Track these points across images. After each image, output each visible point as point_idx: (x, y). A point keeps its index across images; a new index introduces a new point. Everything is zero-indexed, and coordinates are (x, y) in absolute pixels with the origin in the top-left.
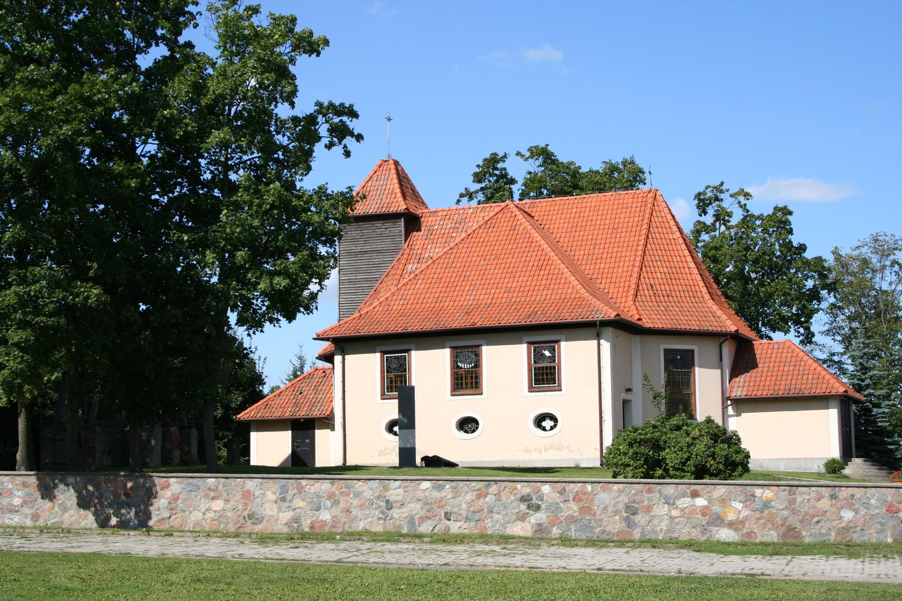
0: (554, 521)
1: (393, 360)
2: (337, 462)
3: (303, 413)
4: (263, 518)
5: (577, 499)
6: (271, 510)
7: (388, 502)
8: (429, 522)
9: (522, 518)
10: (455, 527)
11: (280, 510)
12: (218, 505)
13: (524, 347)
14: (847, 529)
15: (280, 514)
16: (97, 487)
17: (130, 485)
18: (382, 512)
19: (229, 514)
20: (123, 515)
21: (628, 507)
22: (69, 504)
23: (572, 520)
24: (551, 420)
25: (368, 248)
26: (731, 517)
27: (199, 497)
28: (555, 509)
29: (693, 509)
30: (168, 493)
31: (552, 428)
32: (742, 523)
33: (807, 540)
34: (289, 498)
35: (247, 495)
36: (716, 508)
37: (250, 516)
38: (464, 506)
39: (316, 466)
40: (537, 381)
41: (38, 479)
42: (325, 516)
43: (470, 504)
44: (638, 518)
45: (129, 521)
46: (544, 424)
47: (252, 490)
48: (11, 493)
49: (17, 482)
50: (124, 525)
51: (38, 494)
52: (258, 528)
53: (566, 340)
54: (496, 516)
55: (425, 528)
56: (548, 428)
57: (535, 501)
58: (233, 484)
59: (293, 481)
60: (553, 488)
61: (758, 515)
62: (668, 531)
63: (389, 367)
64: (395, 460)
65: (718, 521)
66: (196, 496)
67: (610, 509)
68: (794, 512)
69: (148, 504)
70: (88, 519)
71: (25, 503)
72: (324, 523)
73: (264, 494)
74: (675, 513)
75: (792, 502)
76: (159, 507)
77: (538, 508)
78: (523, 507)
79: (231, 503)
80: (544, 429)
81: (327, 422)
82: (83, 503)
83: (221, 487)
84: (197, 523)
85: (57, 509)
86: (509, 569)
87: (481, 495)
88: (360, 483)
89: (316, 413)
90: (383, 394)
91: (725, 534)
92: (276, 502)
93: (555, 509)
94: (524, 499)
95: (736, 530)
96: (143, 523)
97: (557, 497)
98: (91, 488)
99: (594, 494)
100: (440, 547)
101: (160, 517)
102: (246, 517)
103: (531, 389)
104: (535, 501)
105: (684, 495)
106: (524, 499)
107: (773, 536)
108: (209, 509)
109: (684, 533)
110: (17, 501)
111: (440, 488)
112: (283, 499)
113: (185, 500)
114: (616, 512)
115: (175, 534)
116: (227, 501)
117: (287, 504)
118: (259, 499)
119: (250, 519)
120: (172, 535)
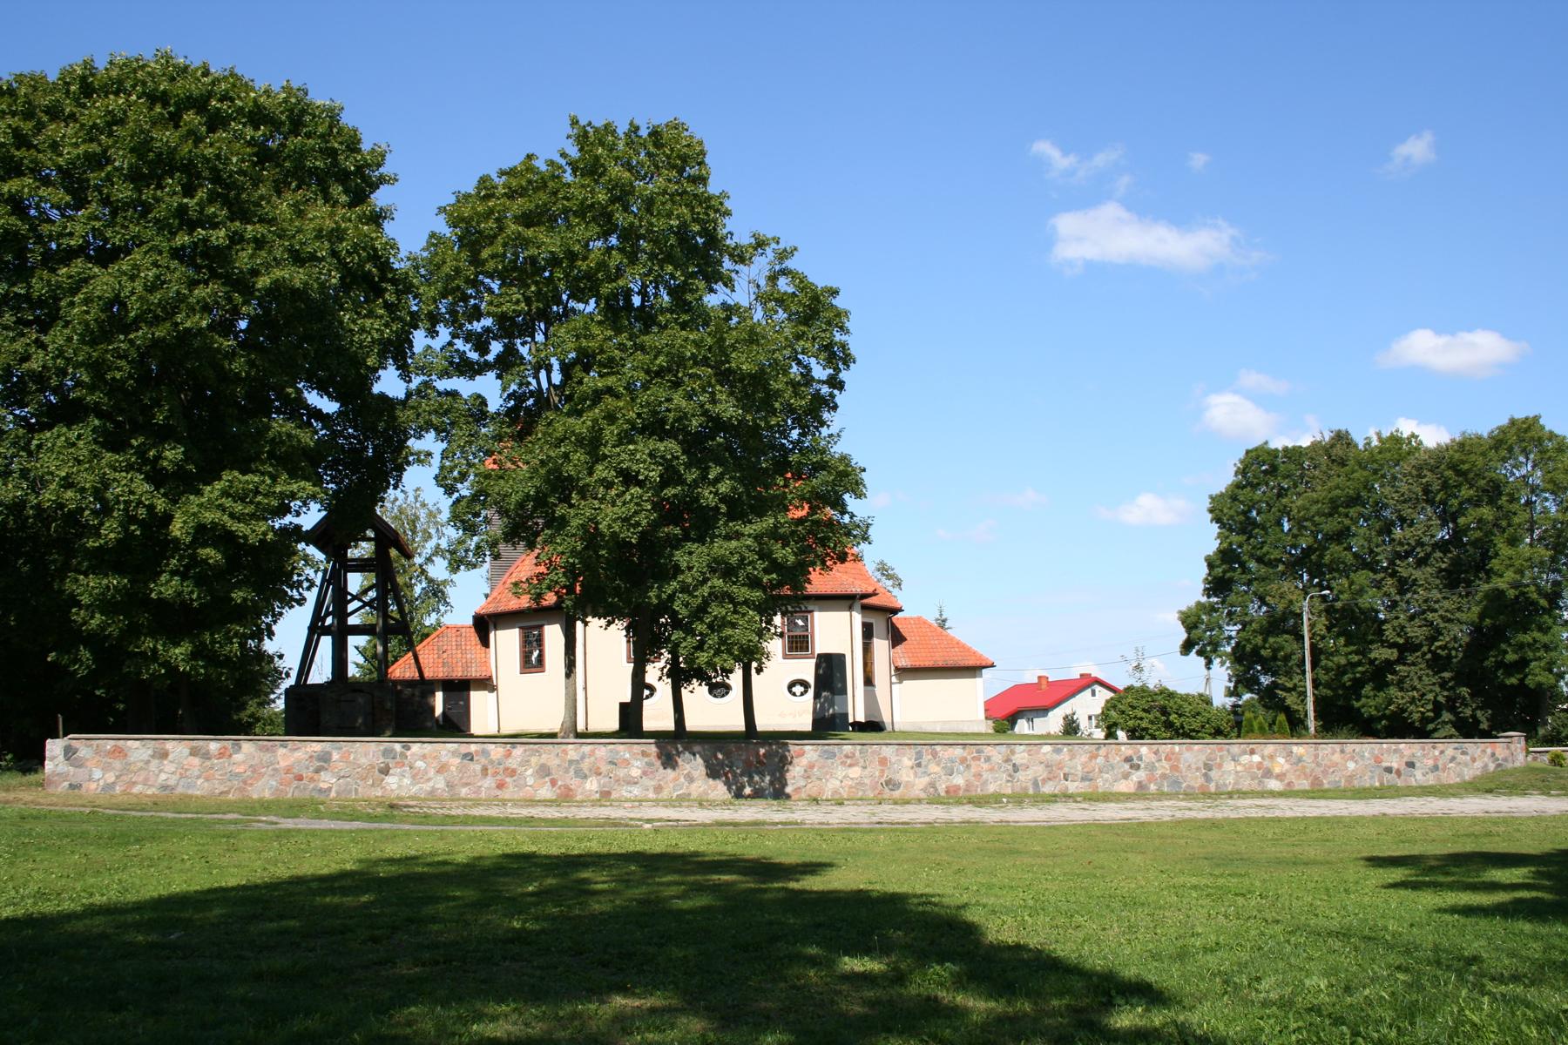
0: (1151, 779)
2: (493, 730)
3: (458, 673)
5: (1168, 758)
6: (908, 776)
7: (1014, 765)
8: (1051, 783)
9: (1126, 776)
10: (1072, 787)
11: (916, 774)
12: (855, 772)
13: (517, 630)
14: (1351, 777)
16: (727, 755)
17: (762, 751)
18: (1010, 776)
19: (867, 781)
21: (1205, 764)
22: (696, 774)
23: (1164, 776)
26: (1277, 770)
28: (1151, 768)
29: (1251, 764)
31: (802, 694)
32: (1284, 775)
33: (1326, 786)
34: (923, 763)
35: (883, 762)
36: (1267, 763)
37: (888, 783)
38: (1079, 768)
40: (791, 649)
41: (658, 747)
42: (959, 780)
43: (1084, 765)
44: (1213, 774)
45: (763, 790)
46: (794, 689)
48: (627, 763)
50: (758, 794)
51: (658, 763)
52: (897, 794)
53: (821, 610)
54: (1106, 776)
55: (1047, 789)
57: (1135, 761)
59: (550, 746)
60: (1150, 749)
61: (1295, 767)
62: (1235, 784)
64: (613, 724)
65: (1268, 773)
67: (1193, 766)
68: (1318, 765)
70: (719, 790)
71: (645, 773)
72: (957, 788)
74: (1239, 768)
75: (1316, 756)
76: (795, 776)
77: (1138, 767)
78: (1127, 766)
79: (869, 769)
80: (794, 694)
81: (486, 684)
82: (713, 773)
83: (857, 754)
84: (835, 792)
85: (682, 780)
87: (1094, 757)
88: (989, 748)
89: (474, 673)
91: (1274, 785)
93: (1151, 768)
94: (1128, 759)
95: (1281, 781)
96: (779, 793)
97: (1153, 758)
98: (720, 756)
99: (1180, 753)
100: (898, 807)
103: (785, 657)
104: (1135, 761)
105: (1244, 753)
106: (1128, 759)
107: (1305, 784)
108: (846, 777)
109: (1246, 784)
110: (635, 772)
111: (1058, 751)
112: (919, 765)
113: (822, 767)
114: (1198, 769)
116: (865, 768)
117: (922, 770)
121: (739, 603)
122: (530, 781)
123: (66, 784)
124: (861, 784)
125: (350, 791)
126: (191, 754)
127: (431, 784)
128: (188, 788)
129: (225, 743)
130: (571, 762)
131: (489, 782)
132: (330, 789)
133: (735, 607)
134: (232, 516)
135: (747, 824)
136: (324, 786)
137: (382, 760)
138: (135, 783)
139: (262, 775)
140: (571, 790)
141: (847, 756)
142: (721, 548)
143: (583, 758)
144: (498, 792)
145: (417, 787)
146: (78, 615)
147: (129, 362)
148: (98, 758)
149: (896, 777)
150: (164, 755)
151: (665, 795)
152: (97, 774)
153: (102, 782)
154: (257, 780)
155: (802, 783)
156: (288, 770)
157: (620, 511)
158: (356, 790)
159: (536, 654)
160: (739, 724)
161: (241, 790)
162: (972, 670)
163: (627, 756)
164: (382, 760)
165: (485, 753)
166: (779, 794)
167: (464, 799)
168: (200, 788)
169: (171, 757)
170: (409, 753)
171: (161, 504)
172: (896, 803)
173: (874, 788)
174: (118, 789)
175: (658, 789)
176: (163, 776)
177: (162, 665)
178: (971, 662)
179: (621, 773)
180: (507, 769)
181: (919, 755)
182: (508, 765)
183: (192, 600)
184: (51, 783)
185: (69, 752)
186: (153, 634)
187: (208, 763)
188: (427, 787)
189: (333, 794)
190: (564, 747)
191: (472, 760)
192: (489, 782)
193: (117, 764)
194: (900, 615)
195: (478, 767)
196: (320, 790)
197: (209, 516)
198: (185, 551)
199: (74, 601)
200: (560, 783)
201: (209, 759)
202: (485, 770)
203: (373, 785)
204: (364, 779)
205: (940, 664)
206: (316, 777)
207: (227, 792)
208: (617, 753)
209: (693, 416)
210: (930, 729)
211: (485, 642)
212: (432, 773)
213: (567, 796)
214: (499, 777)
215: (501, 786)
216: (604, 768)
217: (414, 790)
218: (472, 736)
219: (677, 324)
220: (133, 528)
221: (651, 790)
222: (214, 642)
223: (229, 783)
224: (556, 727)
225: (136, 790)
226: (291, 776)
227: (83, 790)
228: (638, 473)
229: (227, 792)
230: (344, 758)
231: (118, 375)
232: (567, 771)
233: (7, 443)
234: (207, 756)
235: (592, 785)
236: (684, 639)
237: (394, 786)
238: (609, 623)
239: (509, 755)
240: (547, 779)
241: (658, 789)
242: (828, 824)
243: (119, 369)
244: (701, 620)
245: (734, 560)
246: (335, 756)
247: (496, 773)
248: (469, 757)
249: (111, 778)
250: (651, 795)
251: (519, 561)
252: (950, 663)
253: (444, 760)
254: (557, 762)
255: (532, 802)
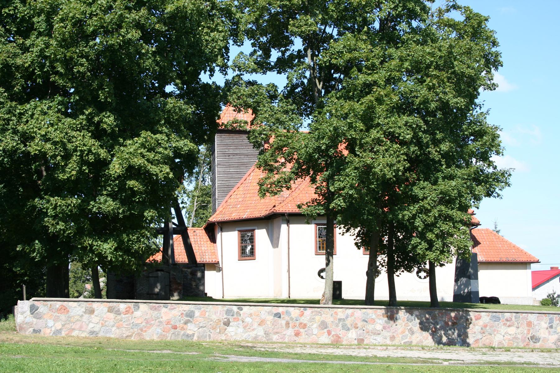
1: (323, 230)
4: (540, 339)
15: (550, 336)
19: (519, 336)
20: (449, 335)
24: (425, 272)
25: (237, 152)
27: (500, 325)
30: (481, 322)
34: (554, 326)
35: (529, 324)
37: (532, 338)
39: (364, 299)
46: (420, 274)
47: (532, 321)
49: (379, 314)
50: (451, 343)
52: (538, 345)
56: (423, 277)
58: (521, 317)
59: (328, 309)
63: (321, 234)
66: (498, 324)
69: (467, 327)
70: (427, 338)
71: (384, 328)
73: (539, 324)
79: (520, 329)
80: (420, 277)
82: (424, 327)
83: (513, 318)
84: (500, 343)
85: (407, 332)
86: (539, 366)
90: (316, 251)
92: (547, 328)
101: (475, 339)
102: (530, 338)
110: (379, 327)
112: (551, 327)
115: (512, 350)
116: (518, 328)
118: (537, 327)
119: (531, 339)
120: (509, 351)
121: (456, 222)
122: (315, 331)
123: (31, 329)
124: (516, 338)
125: (206, 337)
126: (108, 312)
127: (255, 332)
128: (107, 333)
129: (130, 304)
130: (340, 320)
131: (290, 332)
132: (193, 334)
133: (453, 223)
134: (148, 160)
135: (505, 363)
136: (190, 333)
137: (225, 316)
138: (74, 329)
139: (152, 325)
140: (339, 337)
141: (507, 320)
142: (443, 185)
143: (347, 317)
144: (296, 338)
145: (247, 334)
146: (48, 221)
147: (87, 60)
148: (51, 313)
149: (537, 335)
150: (92, 312)
151: (396, 342)
152: (51, 323)
153: (53, 329)
154: (149, 328)
155: (480, 336)
156: (168, 323)
157: (389, 160)
158: (209, 335)
159: (249, 248)
160: (427, 298)
161: (139, 334)
162: (525, 264)
163: (374, 317)
164: (225, 316)
165: (288, 313)
166: (464, 343)
167: (274, 343)
168: (114, 333)
169: (96, 313)
170: (241, 312)
171: (103, 153)
172: (542, 351)
173: (523, 341)
174: (63, 334)
175: (393, 338)
176: (91, 325)
177: (97, 255)
178: (524, 259)
179: (370, 327)
180: (301, 324)
181: (551, 321)
182: (301, 321)
183: (118, 213)
184: (21, 328)
185: (33, 309)
186: (90, 235)
187: (119, 317)
188: (253, 334)
189: (195, 338)
190: (335, 310)
191: (280, 317)
192: (290, 332)
193: (63, 317)
194: (479, 227)
195: (284, 322)
196: (188, 336)
197: (138, 161)
198: (114, 181)
199: (43, 214)
200: (333, 333)
201: (120, 314)
202: (288, 324)
203: (220, 333)
204: (214, 329)
205: (504, 260)
206: (185, 327)
207: (131, 336)
208: (368, 314)
209: (432, 101)
210: (520, 303)
211: (213, 239)
212: (255, 325)
213: (337, 341)
214: (296, 329)
215: (297, 334)
216: (360, 324)
217: (245, 336)
218: (211, 299)
219: (414, 41)
220: (84, 168)
221: (388, 338)
222: (129, 240)
223: (131, 330)
224: (317, 296)
225: (75, 333)
226: (170, 326)
227: (42, 333)
228: (400, 134)
229: (131, 336)
230: (203, 314)
231: (82, 69)
232: (337, 326)
233: (3, 110)
234: (118, 313)
235: (352, 335)
236: (420, 244)
237: (233, 334)
238: (347, 231)
239: (302, 315)
240: (325, 330)
241: (393, 338)
242: (553, 365)
243: (82, 65)
244: (431, 231)
245: (454, 193)
246: (197, 313)
247: (295, 326)
248: (278, 315)
249: (59, 326)
250: (388, 342)
251: (235, 188)
252: (510, 259)
253: (263, 317)
254: (332, 319)
255: (409, 346)
